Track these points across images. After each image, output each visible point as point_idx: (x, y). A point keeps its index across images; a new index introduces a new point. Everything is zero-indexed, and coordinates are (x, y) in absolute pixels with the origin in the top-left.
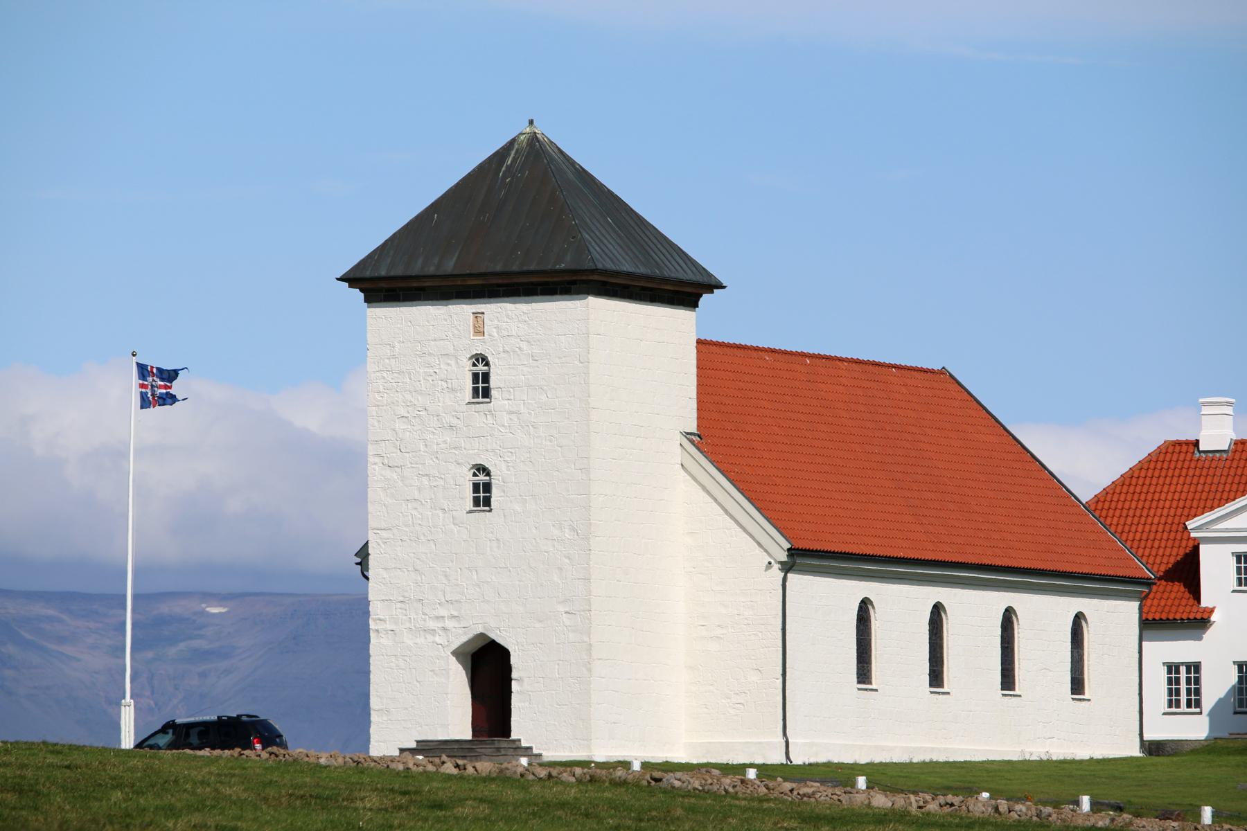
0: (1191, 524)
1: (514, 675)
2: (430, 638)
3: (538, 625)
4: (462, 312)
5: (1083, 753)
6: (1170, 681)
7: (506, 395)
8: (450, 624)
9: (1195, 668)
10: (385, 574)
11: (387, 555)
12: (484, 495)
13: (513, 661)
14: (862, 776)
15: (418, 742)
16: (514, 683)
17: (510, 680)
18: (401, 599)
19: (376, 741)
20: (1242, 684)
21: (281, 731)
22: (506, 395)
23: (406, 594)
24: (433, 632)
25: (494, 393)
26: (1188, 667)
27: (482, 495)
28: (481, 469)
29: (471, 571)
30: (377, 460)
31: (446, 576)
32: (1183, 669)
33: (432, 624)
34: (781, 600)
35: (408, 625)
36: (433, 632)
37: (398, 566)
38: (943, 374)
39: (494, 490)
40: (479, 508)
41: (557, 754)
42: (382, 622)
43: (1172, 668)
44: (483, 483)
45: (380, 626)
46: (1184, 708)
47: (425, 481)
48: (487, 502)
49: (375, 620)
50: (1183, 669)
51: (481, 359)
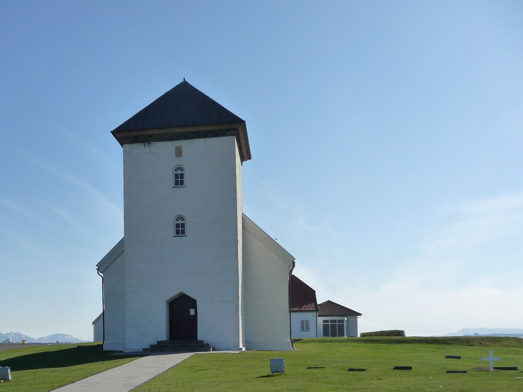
9: (307, 322)
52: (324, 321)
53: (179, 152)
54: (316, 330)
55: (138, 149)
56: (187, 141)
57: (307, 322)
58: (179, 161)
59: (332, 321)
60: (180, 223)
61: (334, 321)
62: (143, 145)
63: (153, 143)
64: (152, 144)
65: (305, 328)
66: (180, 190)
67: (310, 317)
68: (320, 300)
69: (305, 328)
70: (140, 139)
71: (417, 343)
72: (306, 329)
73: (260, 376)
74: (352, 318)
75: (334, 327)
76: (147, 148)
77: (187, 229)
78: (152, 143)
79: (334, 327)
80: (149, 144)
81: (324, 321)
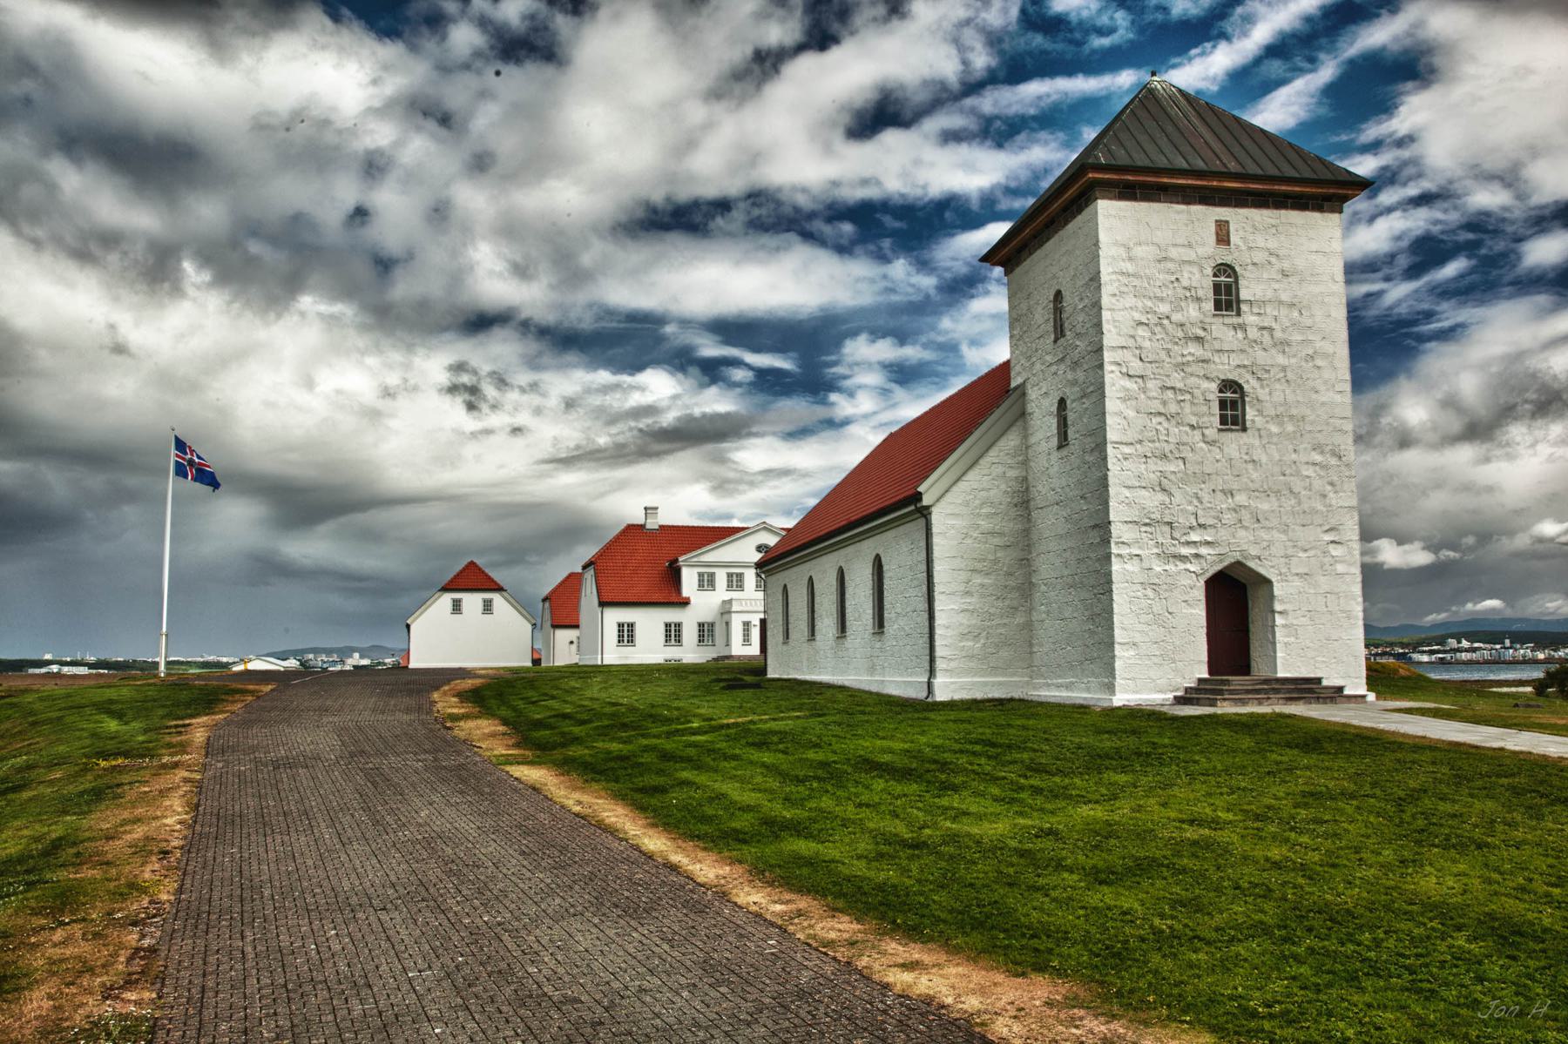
0: (680, 559)
2: (1182, 566)
3: (1301, 554)
4: (1206, 217)
5: (14, 658)
6: (619, 631)
7: (1256, 310)
8: (1204, 551)
10: (1127, 493)
11: (1129, 473)
15: (354, 666)
18: (1147, 521)
19: (1122, 679)
21: (1364, 659)
22: (1256, 310)
23: (1153, 516)
24: (1183, 558)
28: (1229, 385)
29: (1225, 494)
30: (1113, 368)
31: (1198, 498)
32: (626, 626)
33: (1185, 551)
35: (1155, 550)
36: (1183, 558)
37: (1144, 485)
41: (1070, 694)
42: (1126, 546)
43: (620, 625)
45: (1125, 551)
46: (673, 642)
47: (1170, 394)
49: (1117, 543)
51: (1224, 269)
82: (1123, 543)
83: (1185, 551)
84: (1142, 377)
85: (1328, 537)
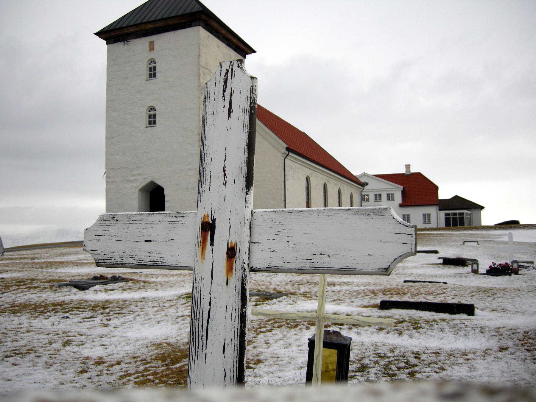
1: (166, 199)
9: (429, 215)
12: (152, 118)
13: (166, 193)
14: (509, 238)
16: (166, 203)
17: (164, 201)
18: (118, 167)
20: (459, 215)
25: (157, 74)
26: (392, 194)
27: (152, 120)
28: (153, 109)
32: (378, 195)
34: (255, 165)
36: (130, 181)
38: (456, 197)
39: (157, 116)
40: (151, 126)
43: (424, 215)
44: (457, 226)
48: (155, 122)
50: (378, 195)
52: (446, 214)
53: (152, 47)
54: (437, 223)
55: (119, 47)
56: (228, 47)
57: (429, 215)
58: (152, 55)
59: (460, 214)
60: (152, 114)
61: (455, 214)
62: (123, 43)
63: (131, 40)
64: (130, 41)
65: (427, 221)
66: (153, 81)
67: (432, 211)
68: (444, 194)
69: (427, 221)
70: (120, 38)
71: (63, 267)
72: (428, 222)
73: (431, 263)
74: (474, 212)
75: (455, 219)
76: (126, 45)
77: (158, 119)
78: (130, 40)
79: (455, 219)
80: (128, 42)
81: (446, 214)
82: (110, 177)
83: (132, 178)
84: (118, 111)
85: (187, 168)
